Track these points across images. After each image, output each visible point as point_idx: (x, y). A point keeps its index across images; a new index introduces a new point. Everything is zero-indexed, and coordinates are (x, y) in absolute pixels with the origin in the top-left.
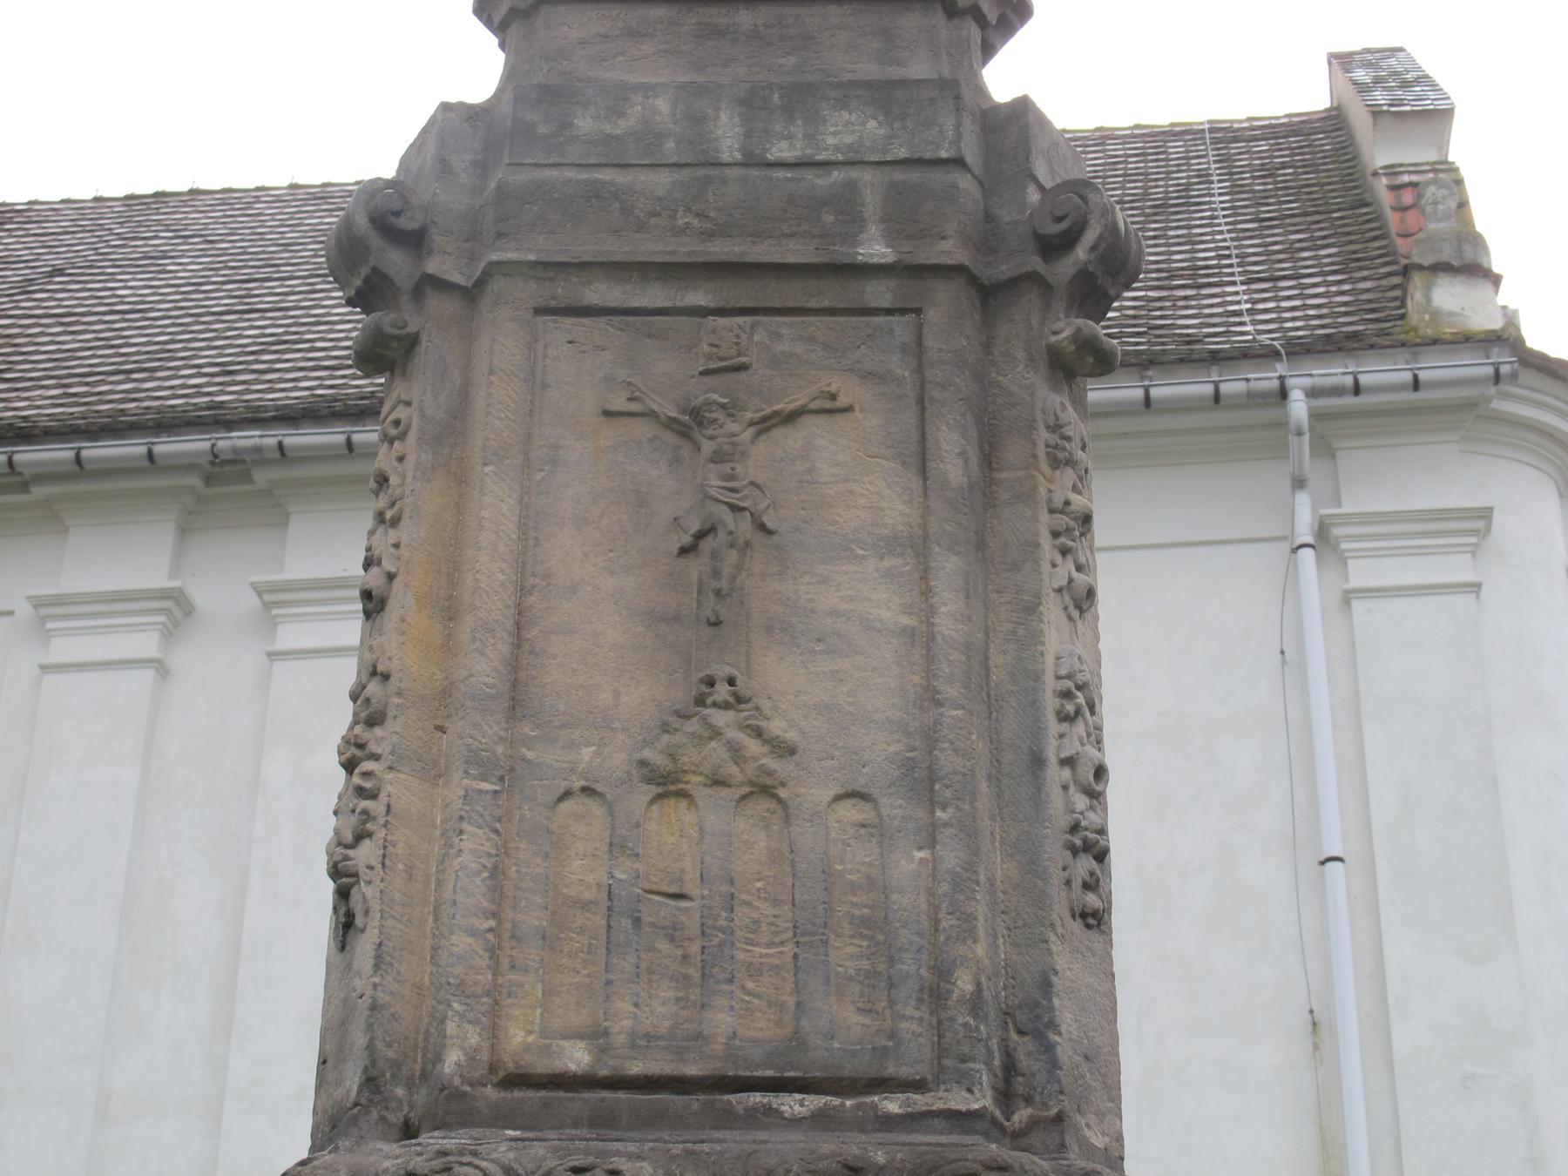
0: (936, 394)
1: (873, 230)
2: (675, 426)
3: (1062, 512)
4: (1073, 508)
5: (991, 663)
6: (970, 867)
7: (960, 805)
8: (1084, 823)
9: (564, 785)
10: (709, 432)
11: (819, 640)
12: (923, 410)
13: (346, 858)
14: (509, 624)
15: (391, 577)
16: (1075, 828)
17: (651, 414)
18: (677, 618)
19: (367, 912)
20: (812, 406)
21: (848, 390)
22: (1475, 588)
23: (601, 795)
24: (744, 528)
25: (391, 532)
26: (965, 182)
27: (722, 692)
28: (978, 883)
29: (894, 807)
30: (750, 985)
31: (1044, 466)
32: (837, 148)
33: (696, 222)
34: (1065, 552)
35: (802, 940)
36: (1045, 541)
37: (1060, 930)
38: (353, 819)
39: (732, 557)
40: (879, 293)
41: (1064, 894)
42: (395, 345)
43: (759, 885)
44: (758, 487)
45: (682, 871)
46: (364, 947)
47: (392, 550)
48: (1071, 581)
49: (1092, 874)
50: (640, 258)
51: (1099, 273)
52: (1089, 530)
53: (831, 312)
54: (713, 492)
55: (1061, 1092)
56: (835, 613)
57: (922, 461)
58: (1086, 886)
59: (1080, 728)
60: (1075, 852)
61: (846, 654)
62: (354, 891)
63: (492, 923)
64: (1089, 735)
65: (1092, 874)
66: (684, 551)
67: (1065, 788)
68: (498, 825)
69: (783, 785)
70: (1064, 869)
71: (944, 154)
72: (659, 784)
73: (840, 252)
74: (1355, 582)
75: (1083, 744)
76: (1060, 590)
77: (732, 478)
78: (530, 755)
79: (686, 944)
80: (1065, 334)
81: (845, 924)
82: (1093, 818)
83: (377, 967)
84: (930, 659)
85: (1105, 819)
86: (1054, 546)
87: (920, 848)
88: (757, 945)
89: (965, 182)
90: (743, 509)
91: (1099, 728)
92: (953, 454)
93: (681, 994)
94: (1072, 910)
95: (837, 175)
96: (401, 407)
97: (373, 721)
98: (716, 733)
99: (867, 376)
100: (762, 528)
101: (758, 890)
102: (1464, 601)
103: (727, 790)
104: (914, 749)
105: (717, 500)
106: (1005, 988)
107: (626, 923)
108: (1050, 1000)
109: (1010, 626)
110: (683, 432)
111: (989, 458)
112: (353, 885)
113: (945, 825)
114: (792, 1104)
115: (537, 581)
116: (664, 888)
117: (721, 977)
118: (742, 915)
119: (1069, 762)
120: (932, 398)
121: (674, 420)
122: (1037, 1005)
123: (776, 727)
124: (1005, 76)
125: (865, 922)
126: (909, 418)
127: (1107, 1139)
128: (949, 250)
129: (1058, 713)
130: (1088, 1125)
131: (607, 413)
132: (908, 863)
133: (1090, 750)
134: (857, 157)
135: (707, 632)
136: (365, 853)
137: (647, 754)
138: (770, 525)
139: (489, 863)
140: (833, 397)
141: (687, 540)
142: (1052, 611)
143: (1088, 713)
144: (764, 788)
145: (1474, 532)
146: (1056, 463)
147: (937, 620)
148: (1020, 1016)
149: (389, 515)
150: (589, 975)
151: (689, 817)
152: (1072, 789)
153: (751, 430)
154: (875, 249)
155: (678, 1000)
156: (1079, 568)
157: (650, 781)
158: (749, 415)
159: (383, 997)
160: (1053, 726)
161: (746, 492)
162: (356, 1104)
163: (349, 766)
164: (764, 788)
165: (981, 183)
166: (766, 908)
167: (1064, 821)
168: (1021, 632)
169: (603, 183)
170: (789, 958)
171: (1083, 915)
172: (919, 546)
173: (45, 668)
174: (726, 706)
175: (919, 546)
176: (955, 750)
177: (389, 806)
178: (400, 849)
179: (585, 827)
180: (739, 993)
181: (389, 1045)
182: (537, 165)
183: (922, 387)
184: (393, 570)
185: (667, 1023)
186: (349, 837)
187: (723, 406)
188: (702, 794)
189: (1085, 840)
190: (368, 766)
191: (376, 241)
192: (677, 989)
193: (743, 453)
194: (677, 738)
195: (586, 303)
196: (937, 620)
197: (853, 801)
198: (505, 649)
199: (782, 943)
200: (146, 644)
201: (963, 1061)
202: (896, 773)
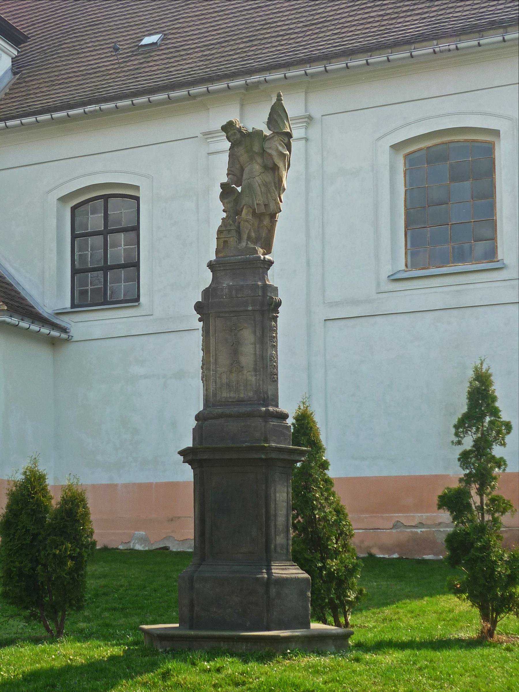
57: (255, 333)
111: (263, 333)
154: (250, 308)
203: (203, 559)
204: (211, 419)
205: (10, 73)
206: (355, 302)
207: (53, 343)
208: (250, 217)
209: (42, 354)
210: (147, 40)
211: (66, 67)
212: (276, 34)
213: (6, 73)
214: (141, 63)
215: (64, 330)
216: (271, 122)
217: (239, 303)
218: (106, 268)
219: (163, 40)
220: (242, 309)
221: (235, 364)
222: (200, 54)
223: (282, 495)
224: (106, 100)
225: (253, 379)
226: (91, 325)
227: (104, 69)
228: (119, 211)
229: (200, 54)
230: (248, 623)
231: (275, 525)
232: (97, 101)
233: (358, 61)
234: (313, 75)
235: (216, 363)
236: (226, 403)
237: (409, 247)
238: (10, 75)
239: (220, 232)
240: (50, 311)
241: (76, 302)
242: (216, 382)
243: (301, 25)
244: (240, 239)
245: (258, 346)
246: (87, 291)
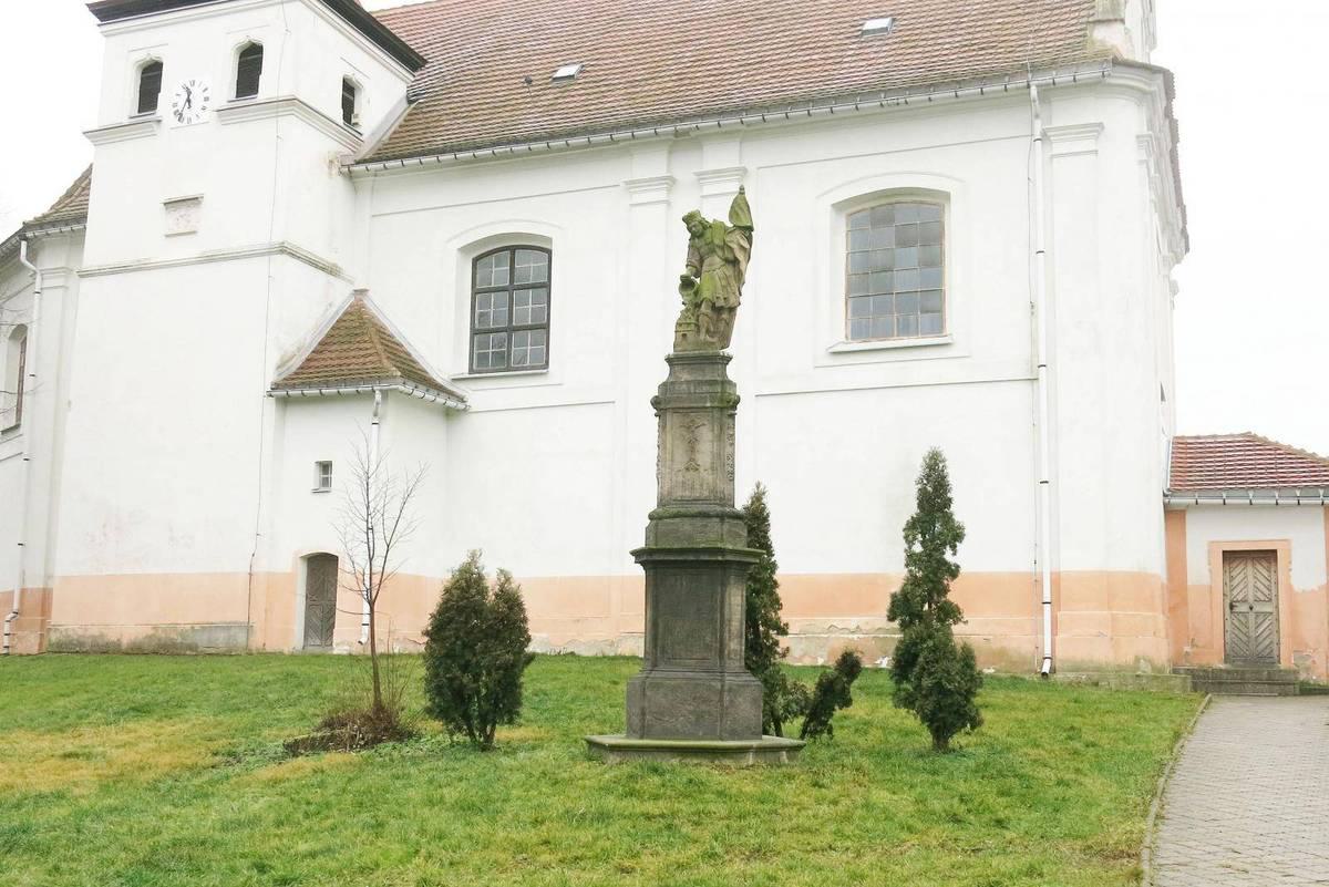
22: (1096, 152)
29: (710, 472)
57: (713, 430)
61: (705, 455)
74: (1055, 152)
102: (1092, 157)
111: (721, 429)
128: (716, 404)
132: (711, 477)
145: (1097, 131)
154: (708, 405)
172: (712, 441)
173: (632, 205)
175: (712, 441)
200: (662, 195)
203: (655, 665)
204: (666, 518)
205: (405, 101)
207: (449, 413)
208: (709, 311)
209: (433, 428)
210: (563, 72)
211: (470, 98)
212: (708, 73)
213: (400, 101)
214: (557, 98)
215: (462, 400)
216: (733, 214)
217: (697, 395)
218: (511, 330)
219: (581, 72)
220: (701, 405)
221: (692, 466)
222: (623, 92)
223: (736, 599)
224: (517, 141)
225: (711, 477)
226: (485, 395)
227: (514, 102)
228: (528, 266)
229: (623, 92)
230: (701, 734)
231: (730, 630)
232: (509, 142)
233: (800, 113)
234: (749, 125)
236: (683, 501)
237: (849, 317)
238: (405, 104)
239: (679, 324)
240: (446, 377)
241: (474, 367)
243: (736, 64)
244: (698, 331)
246: (486, 355)
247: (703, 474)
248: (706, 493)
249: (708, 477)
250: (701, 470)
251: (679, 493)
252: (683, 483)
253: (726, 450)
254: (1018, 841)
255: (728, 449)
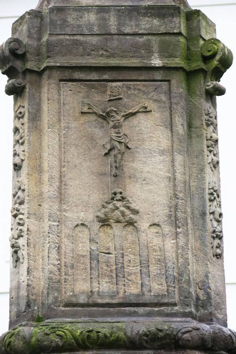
0: (175, 106)
1: (156, 55)
2: (102, 117)
3: (210, 140)
4: (213, 138)
5: (191, 185)
6: (187, 244)
7: (184, 227)
8: (216, 230)
9: (76, 223)
10: (112, 119)
11: (144, 180)
12: (171, 111)
13: (16, 243)
14: (58, 176)
15: (22, 160)
16: (214, 232)
17: (95, 113)
18: (105, 174)
19: (23, 258)
20: (140, 110)
21: (151, 105)
23: (87, 226)
24: (123, 147)
25: (21, 146)
26: (182, 40)
27: (119, 197)
28: (189, 249)
29: (167, 229)
30: (129, 278)
31: (205, 127)
32: (145, 29)
33: (105, 53)
34: (210, 151)
35: (142, 265)
36: (206, 149)
37: (211, 261)
38: (18, 232)
39: (119, 156)
40: (158, 76)
41: (211, 251)
42: (19, 89)
43: (130, 250)
44: (126, 135)
45: (109, 246)
46: (24, 268)
47: (22, 152)
48: (212, 159)
49: (218, 244)
50: (89, 65)
51: (220, 67)
52: (217, 144)
53: (145, 81)
54: (114, 138)
55: (211, 305)
56: (148, 172)
57: (171, 126)
58: (217, 247)
59: (215, 203)
60: (214, 238)
62: (19, 252)
63: (59, 262)
64: (217, 204)
65: (218, 244)
66: (106, 154)
67: (211, 220)
68: (59, 235)
69: (136, 222)
70: (211, 244)
71: (175, 31)
72: (102, 222)
73: (146, 62)
75: (216, 207)
76: (209, 163)
77: (119, 133)
78: (66, 215)
79: (112, 267)
80: (211, 87)
81: (153, 260)
82: (219, 229)
83: (28, 274)
84: (175, 186)
85: (222, 228)
86: (208, 150)
87: (173, 240)
88: (130, 267)
89: (182, 40)
90: (122, 143)
91: (220, 202)
92: (180, 128)
93: (110, 281)
94: (213, 255)
95: (145, 37)
96: (21, 108)
97: (21, 203)
98: (117, 208)
99: (155, 101)
100: (127, 147)
101: (130, 251)
103: (121, 224)
104: (171, 212)
105: (115, 140)
106: (196, 277)
107: (95, 262)
108: (208, 280)
109: (196, 174)
110: (104, 118)
111: (190, 126)
112: (18, 250)
113: (180, 233)
114: (141, 310)
115: (65, 164)
116: (105, 251)
117: (121, 276)
118: (126, 259)
119: (213, 213)
120: (174, 108)
121: (102, 115)
122: (205, 282)
123: (133, 206)
124: (217, 96)
125: (159, 260)
126: (167, 114)
127: (223, 316)
128: (178, 62)
129: (209, 199)
130: (218, 313)
131: (82, 113)
133: (218, 209)
134: (151, 32)
135: (113, 178)
136: (22, 242)
137: (99, 214)
138: (130, 147)
139: (57, 245)
140: (146, 108)
141: (107, 151)
142: (208, 170)
143: (217, 198)
144: (131, 223)
146: (208, 125)
147: (176, 174)
148: (200, 284)
149: (20, 141)
150: (85, 276)
151: (110, 231)
152: (213, 221)
153: (123, 118)
154: (157, 62)
155: (110, 282)
156: (214, 155)
157: (99, 222)
158: (123, 114)
159: (30, 283)
160: (208, 203)
161: (122, 137)
162: (25, 312)
163: (15, 216)
164: (131, 223)
165: (186, 38)
166: (132, 257)
167: (212, 230)
168: (199, 176)
169: (77, 40)
170: (139, 270)
171: (216, 255)
172: (172, 151)
174: (120, 200)
176: (182, 212)
177: (28, 229)
178: (32, 240)
179: (84, 235)
180: (126, 280)
181: (32, 295)
182: (57, 34)
183: (171, 104)
184: (23, 159)
185: (107, 288)
186: (16, 236)
187: (115, 111)
188: (114, 225)
189: (217, 235)
190: (20, 216)
191: (12, 58)
192: (109, 279)
193: (121, 126)
194: (107, 210)
195: (74, 78)
196: (176, 174)
197: (155, 226)
198: (57, 184)
199: (137, 266)
201: (186, 298)
202: (166, 219)
206: (61, 323)
220: (135, 62)
221: (116, 213)
225: (169, 244)
235: (61, 197)
242: (59, 248)
245: (179, 158)
247: (149, 235)
248: (157, 287)
249: (165, 245)
250: (143, 224)
251: (81, 287)
252: (93, 257)
253: (207, 180)
254: (195, 281)
255: (209, 177)
